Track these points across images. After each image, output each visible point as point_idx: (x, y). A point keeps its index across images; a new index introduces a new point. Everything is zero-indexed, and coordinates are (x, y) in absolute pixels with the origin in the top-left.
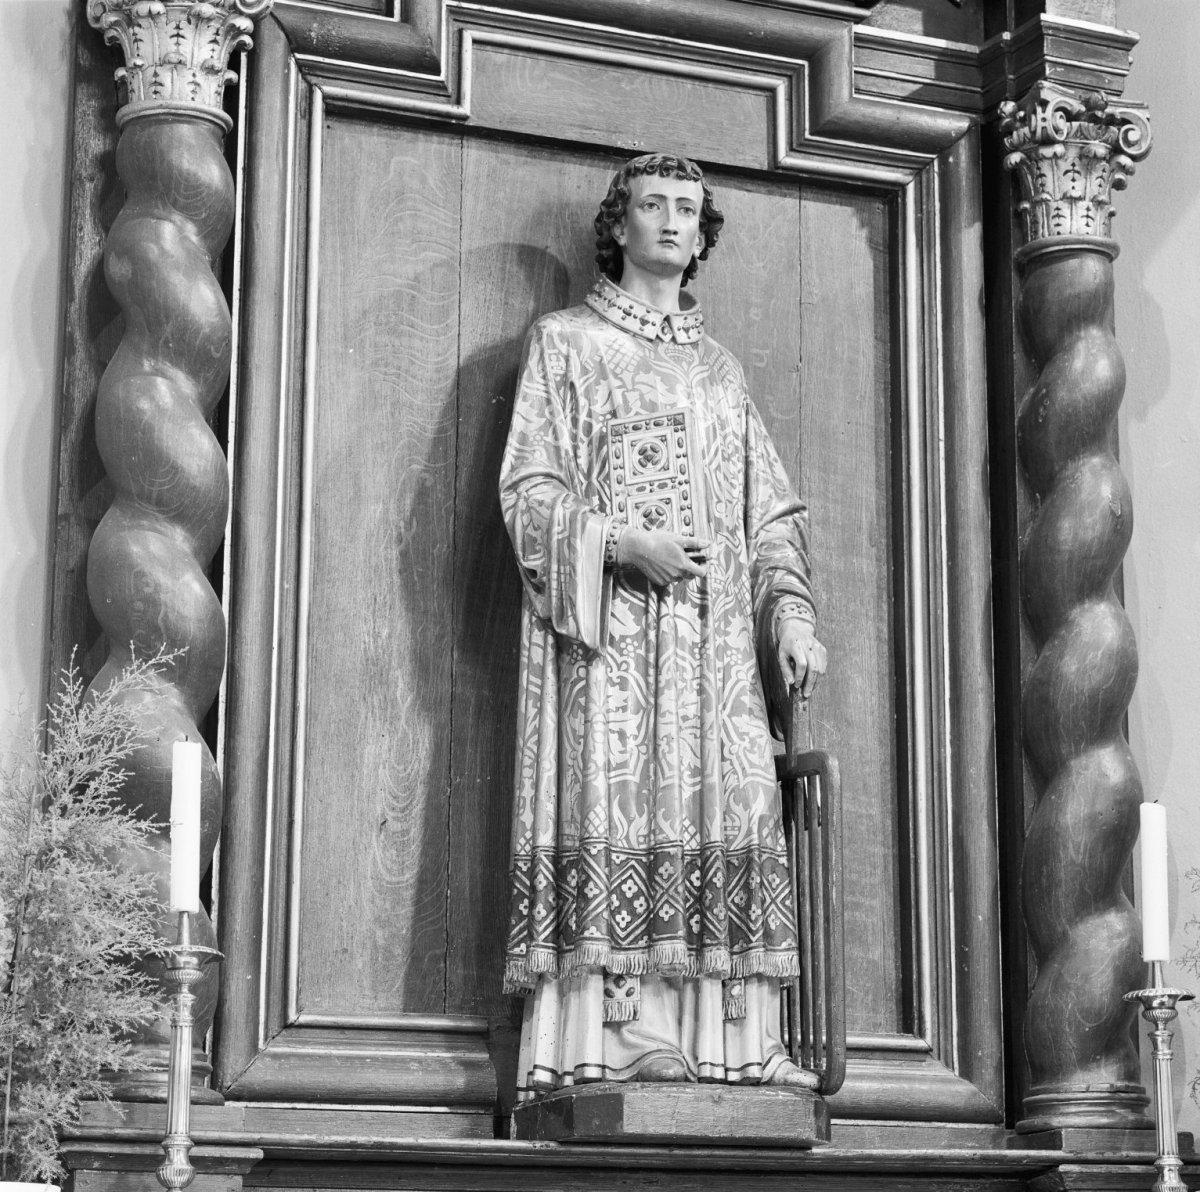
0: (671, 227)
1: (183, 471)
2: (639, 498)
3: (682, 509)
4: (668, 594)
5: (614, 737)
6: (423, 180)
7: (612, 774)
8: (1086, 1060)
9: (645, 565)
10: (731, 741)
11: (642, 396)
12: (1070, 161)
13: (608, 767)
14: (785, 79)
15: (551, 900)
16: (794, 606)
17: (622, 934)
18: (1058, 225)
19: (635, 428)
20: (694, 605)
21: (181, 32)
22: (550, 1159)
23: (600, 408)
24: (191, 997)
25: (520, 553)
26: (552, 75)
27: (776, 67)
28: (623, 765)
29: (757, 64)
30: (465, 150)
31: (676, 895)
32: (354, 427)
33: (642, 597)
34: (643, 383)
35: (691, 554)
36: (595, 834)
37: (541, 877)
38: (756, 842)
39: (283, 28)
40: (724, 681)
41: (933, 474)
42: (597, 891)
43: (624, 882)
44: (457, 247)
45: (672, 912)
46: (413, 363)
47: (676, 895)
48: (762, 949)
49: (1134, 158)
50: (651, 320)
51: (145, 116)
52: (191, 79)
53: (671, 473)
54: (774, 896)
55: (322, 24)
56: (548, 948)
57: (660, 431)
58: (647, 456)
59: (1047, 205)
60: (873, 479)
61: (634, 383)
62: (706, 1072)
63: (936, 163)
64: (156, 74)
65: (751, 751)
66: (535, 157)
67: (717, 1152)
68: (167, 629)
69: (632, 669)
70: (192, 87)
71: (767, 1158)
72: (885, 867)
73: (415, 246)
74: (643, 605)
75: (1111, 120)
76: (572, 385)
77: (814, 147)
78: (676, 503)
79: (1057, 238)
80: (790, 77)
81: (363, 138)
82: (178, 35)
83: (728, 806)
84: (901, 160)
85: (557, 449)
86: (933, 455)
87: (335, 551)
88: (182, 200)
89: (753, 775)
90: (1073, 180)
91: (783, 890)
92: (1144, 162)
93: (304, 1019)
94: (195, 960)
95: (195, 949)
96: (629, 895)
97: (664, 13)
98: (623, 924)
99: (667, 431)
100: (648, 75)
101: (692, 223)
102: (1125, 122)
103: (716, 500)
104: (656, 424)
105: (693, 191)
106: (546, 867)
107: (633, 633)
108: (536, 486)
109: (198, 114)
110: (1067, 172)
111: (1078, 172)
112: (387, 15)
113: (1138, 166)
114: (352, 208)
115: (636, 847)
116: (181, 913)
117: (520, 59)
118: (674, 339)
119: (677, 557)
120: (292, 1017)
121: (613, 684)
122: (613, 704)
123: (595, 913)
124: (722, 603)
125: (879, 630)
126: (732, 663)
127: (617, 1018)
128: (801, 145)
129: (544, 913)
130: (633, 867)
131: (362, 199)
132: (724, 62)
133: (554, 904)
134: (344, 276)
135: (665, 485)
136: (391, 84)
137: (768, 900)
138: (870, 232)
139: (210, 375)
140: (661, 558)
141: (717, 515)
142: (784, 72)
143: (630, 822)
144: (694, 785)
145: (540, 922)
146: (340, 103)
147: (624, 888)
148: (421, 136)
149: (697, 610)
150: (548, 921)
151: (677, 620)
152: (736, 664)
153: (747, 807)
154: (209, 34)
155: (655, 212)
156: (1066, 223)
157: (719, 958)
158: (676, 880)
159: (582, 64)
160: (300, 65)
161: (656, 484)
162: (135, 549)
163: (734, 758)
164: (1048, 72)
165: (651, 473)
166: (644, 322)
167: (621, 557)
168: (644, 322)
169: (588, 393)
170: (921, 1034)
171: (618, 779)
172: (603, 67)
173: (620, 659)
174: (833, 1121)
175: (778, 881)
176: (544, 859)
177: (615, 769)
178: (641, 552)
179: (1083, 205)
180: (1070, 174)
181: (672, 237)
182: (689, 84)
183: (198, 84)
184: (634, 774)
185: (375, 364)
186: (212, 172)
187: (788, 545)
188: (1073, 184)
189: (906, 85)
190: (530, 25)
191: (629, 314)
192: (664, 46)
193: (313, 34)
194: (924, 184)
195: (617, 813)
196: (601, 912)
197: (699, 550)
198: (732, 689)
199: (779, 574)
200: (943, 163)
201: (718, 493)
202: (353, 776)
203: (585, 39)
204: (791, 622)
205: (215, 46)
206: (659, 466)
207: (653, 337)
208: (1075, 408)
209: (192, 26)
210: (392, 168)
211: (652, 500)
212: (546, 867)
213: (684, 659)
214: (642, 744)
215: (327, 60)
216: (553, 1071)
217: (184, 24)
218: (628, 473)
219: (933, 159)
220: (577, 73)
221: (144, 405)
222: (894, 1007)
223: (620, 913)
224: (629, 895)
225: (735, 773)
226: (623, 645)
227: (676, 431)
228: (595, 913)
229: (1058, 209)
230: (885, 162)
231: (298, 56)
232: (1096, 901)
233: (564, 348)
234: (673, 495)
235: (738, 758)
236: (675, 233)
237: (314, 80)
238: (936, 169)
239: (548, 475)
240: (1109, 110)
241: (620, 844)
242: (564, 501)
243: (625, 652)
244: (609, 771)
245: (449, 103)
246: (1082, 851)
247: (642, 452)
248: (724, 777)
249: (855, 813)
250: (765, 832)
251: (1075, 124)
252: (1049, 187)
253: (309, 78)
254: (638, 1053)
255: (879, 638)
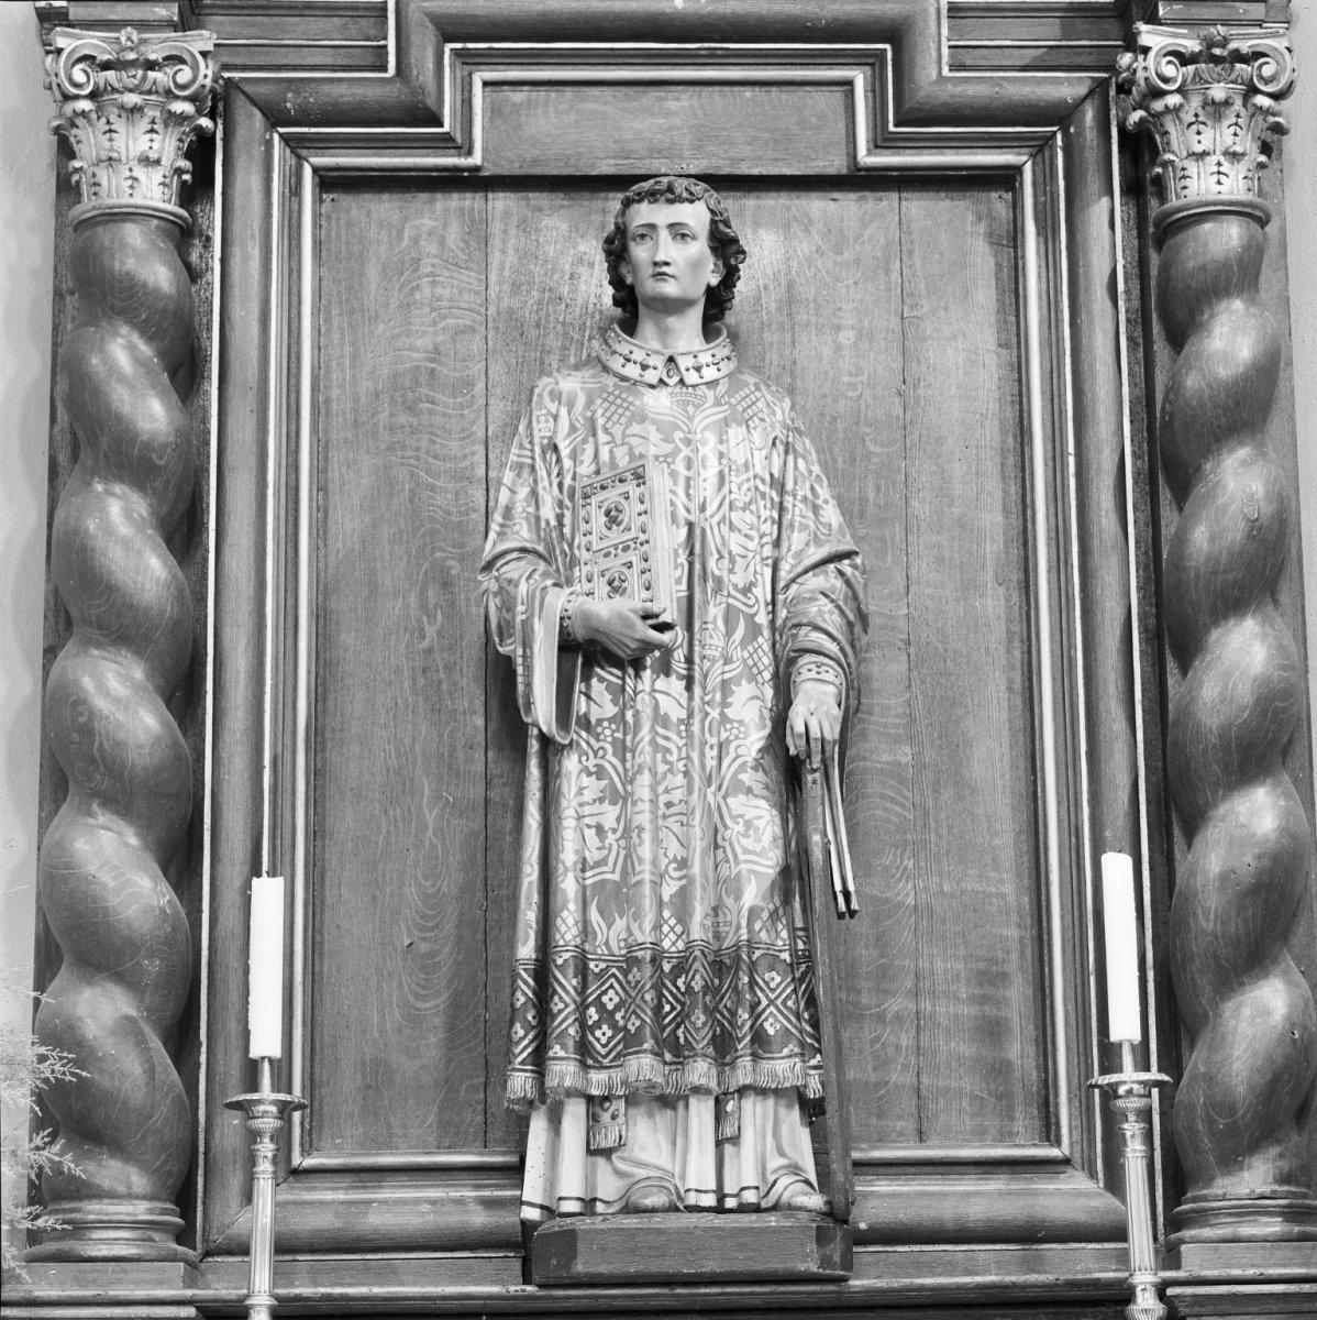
0: (660, 257)
1: (118, 589)
2: (604, 563)
3: (643, 573)
4: (645, 668)
5: (590, 834)
6: (442, 243)
7: (588, 874)
8: (1231, 1160)
9: (604, 639)
10: (726, 826)
11: (631, 449)
12: (1192, 113)
13: (584, 866)
14: (868, 68)
15: (530, 1017)
16: (813, 667)
17: (603, 1051)
18: (1185, 188)
19: (603, 488)
20: (681, 677)
21: (113, 127)
22: (531, 1305)
23: (586, 469)
24: (272, 1146)
25: (497, 640)
26: (580, 106)
27: (852, 56)
28: (602, 862)
29: (830, 56)
30: (490, 203)
31: (643, 1005)
32: (368, 520)
33: (619, 673)
34: (634, 435)
35: (650, 622)
36: (561, 943)
37: (519, 994)
38: (745, 937)
39: (256, 105)
40: (720, 759)
41: (1063, 494)
42: (561, 1006)
43: (605, 992)
44: (483, 310)
45: (638, 1023)
46: (434, 442)
47: (643, 1005)
48: (748, 1058)
49: (1277, 97)
50: (651, 364)
51: (88, 219)
52: (128, 174)
53: (633, 534)
54: (772, 996)
55: (297, 93)
56: (526, 1071)
57: (622, 488)
58: (613, 518)
59: (1173, 167)
60: (1000, 507)
61: (624, 435)
62: (692, 1199)
63: (1059, 136)
64: (94, 175)
65: (746, 836)
66: (573, 198)
67: (728, 1290)
68: (104, 759)
69: (609, 756)
70: (130, 182)
71: (792, 1293)
72: (1022, 952)
73: (434, 315)
74: (620, 682)
75: (1238, 57)
76: (556, 449)
77: (903, 140)
78: (638, 565)
79: (1182, 202)
80: (872, 65)
81: (372, 206)
82: (110, 131)
83: (720, 899)
84: (1016, 139)
85: (538, 519)
86: (1063, 472)
87: (349, 655)
88: (118, 304)
89: (746, 861)
90: (1199, 133)
91: (784, 989)
92: (1292, 97)
93: (309, 1162)
94: (274, 1109)
95: (275, 1096)
96: (610, 1006)
97: (701, 17)
98: (604, 1041)
99: (630, 487)
100: (697, 88)
101: (700, 247)
102: (1257, 55)
103: (716, 556)
104: (621, 481)
105: (695, 215)
106: (526, 983)
107: (610, 715)
108: (508, 563)
109: (133, 210)
110: (1190, 125)
111: (1204, 123)
112: (380, 71)
113: (1284, 104)
114: (361, 285)
115: (617, 953)
116: (263, 1058)
117: (542, 93)
118: (682, 381)
119: (631, 626)
120: (297, 1160)
121: (589, 774)
122: (588, 796)
123: (558, 1031)
124: (720, 671)
125: (1010, 681)
126: (732, 738)
127: (603, 1145)
128: (885, 140)
129: (521, 1033)
130: (614, 975)
131: (373, 272)
132: (789, 61)
133: (534, 1023)
134: (355, 357)
135: (628, 548)
136: (390, 144)
137: (765, 1002)
138: (990, 226)
139: (158, 484)
140: (617, 628)
141: (717, 572)
142: (864, 60)
143: (609, 927)
144: (680, 879)
145: (518, 1043)
146: (335, 174)
147: (605, 999)
148: (439, 195)
149: (684, 682)
150: (526, 1042)
151: (658, 695)
152: (737, 737)
153: (738, 898)
154: (144, 125)
155: (649, 243)
156: (1192, 184)
157: (701, 1071)
158: (643, 987)
159: (618, 88)
160: (285, 138)
161: (621, 547)
162: (88, 683)
163: (727, 844)
164: (1161, 12)
165: (616, 536)
166: (644, 367)
167: (580, 633)
168: (644, 367)
169: (574, 456)
170: (1058, 1143)
171: (596, 879)
172: (640, 89)
173: (596, 745)
174: (855, 1249)
175: (778, 979)
176: (525, 975)
177: (592, 868)
178: (594, 625)
179: (1213, 159)
180: (1194, 127)
181: (665, 269)
182: (748, 93)
183: (136, 179)
184: (613, 872)
185: (391, 448)
186: (159, 274)
187: (821, 596)
188: (1198, 137)
189: (1026, 51)
190: (552, 56)
191: (629, 360)
192: (712, 54)
193: (288, 105)
194: (1047, 162)
195: (594, 916)
196: (566, 1029)
197: (657, 616)
198: (729, 767)
199: (804, 630)
200: (1066, 135)
201: (720, 547)
202: (374, 898)
203: (619, 61)
204: (808, 685)
205: (154, 136)
206: (622, 527)
207: (654, 381)
208: (1200, 399)
209: (124, 120)
210: (406, 235)
211: (614, 564)
212: (526, 983)
213: (667, 738)
214: (622, 837)
215: (313, 130)
216: (542, 1207)
217: (113, 118)
218: (594, 538)
219: (1055, 133)
220: (609, 99)
221: (92, 525)
222: (1036, 1112)
223: (600, 1028)
224: (610, 1006)
225: (728, 861)
226: (599, 730)
227: (638, 486)
228: (558, 1031)
229: (1184, 169)
230: (996, 144)
231: (281, 130)
232: (1237, 975)
233: (553, 407)
234: (633, 557)
235: (731, 844)
236: (667, 264)
237: (304, 152)
238: (1059, 143)
239: (523, 550)
240: (1233, 45)
241: (599, 951)
242: (529, 577)
243: (602, 737)
244: (583, 871)
245: (459, 155)
246: (1212, 917)
247: (608, 513)
248: (716, 866)
249: (983, 893)
250: (757, 926)
251: (1191, 68)
252: (1175, 144)
253: (299, 151)
254: (631, 1180)
255: (1010, 689)
